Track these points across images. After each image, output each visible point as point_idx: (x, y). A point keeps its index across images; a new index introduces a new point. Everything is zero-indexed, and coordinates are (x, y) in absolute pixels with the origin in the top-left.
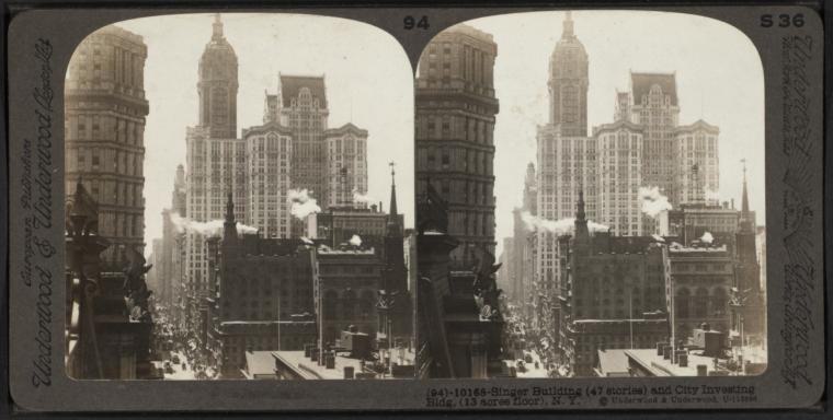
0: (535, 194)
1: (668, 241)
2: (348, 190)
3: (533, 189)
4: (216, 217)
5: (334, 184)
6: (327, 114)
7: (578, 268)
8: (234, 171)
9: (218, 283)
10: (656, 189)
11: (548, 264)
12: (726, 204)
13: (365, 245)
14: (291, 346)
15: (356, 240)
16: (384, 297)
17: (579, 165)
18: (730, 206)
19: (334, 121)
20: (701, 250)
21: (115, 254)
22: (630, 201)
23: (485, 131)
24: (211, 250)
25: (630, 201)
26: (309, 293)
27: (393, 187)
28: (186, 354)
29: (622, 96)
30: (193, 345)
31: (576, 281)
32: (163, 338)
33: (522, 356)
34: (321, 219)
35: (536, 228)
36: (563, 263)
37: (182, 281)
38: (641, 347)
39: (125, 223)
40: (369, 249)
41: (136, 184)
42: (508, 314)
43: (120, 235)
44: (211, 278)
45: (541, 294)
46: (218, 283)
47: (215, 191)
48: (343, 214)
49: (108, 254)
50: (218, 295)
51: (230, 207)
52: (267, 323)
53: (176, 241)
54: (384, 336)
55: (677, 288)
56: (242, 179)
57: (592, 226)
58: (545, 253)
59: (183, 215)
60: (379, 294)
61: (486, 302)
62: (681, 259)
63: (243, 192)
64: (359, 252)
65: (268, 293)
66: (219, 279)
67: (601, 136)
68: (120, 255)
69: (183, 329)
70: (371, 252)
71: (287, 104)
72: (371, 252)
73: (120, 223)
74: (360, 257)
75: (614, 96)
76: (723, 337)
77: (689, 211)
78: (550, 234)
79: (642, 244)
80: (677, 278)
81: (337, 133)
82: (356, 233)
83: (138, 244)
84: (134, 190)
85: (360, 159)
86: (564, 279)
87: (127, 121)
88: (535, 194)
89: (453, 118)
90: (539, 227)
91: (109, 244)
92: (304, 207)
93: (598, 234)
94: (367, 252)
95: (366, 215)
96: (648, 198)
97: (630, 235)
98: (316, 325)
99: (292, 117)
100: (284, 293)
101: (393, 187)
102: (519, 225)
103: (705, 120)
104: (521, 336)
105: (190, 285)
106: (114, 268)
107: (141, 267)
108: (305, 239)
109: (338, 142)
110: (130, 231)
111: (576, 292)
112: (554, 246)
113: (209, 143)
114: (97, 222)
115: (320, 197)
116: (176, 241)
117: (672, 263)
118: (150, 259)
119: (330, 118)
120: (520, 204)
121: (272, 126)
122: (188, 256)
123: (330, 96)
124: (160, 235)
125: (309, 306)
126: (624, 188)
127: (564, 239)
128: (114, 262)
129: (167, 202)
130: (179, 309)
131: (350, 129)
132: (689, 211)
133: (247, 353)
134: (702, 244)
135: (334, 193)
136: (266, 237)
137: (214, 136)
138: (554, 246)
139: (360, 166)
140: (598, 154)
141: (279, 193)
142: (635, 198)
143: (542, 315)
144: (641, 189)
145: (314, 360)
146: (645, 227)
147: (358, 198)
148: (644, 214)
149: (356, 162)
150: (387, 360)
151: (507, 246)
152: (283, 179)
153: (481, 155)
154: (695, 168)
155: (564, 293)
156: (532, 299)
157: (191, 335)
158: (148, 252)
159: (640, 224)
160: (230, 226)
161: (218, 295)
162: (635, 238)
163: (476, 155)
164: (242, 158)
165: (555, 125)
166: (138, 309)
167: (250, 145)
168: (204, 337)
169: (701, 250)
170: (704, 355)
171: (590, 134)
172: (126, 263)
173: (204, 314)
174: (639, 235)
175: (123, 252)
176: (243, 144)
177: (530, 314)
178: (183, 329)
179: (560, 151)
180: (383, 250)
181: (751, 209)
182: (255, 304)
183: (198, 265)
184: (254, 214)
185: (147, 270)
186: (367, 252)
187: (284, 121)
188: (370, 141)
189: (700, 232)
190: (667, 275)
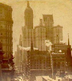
0: (22, 41)
1: (51, 52)
2: (59, 40)
3: (21, 40)
4: (29, 46)
5: (55, 38)
6: (53, 23)
7: (31, 58)
8: (33, 36)
9: (29, 61)
10: (49, 40)
11: (24, 57)
12: (64, 44)
13: (63, 51)
14: (46, 75)
15: (60, 51)
16: (67, 64)
17: (31, 35)
18: (65, 44)
19: (55, 24)
20: (59, 54)
21: (6, 54)
22: (43, 43)
23: (10, 28)
24: (28, 54)
25: (43, 43)
26: (50, 63)
27: (69, 39)
28: (22, 77)
29: (41, 20)
30: (24, 75)
31: (31, 61)
32: (17, 73)
33: (18, 78)
34: (52, 46)
35: (22, 49)
36: (28, 57)
37: (21, 60)
38: (45, 75)
39: (8, 48)
40: (63, 53)
41: (11, 39)
42: (16, 68)
43: (7, 50)
44: (28, 60)
45: (23, 64)
46: (29, 61)
47: (29, 40)
48: (57, 45)
49: (4, 55)
50: (29, 64)
51: (32, 44)
52: (40, 70)
53: (20, 52)
54: (67, 72)
55: (54, 62)
56: (35, 38)
57: (34, 49)
58: (24, 55)
59: (21, 46)
60: (66, 63)
61: (11, 66)
62: (54, 56)
63: (35, 40)
64: (61, 54)
65: (41, 63)
66: (30, 60)
67: (36, 29)
68: (7, 55)
69: (22, 71)
70: (64, 53)
71: (44, 21)
72: (64, 53)
73: (7, 48)
74: (61, 55)
75: (39, 20)
76: (64, 73)
77: (56, 45)
78: (25, 50)
79: (45, 53)
80: (54, 60)
81: (56, 27)
82: (60, 49)
83: (11, 53)
84: (10, 41)
85: (61, 33)
86: (28, 60)
87: (8, 25)
88: (22, 41)
89: (3, 25)
90: (23, 49)
91: (5, 53)
92: (48, 44)
93: (36, 50)
94: (63, 54)
95: (63, 45)
96: (47, 42)
97: (43, 50)
98: (51, 70)
99: (46, 24)
100: (44, 63)
101: (69, 39)
102: (18, 49)
103: (60, 25)
104: (18, 73)
105: (23, 61)
106: (6, 58)
107: (12, 58)
108: (49, 51)
109: (56, 29)
110: (9, 49)
111: (31, 63)
112: (26, 53)
113: (27, 29)
114: (2, 48)
115: (52, 41)
116: (20, 52)
117: (53, 57)
118: (14, 56)
119: (54, 24)
120: (18, 44)
121: (41, 26)
122: (23, 55)
123: (54, 19)
124: (16, 50)
125: (50, 66)
126: (41, 40)
127: (28, 52)
128: (6, 57)
129: (18, 43)
130: (21, 67)
131: (59, 26)
132: (56, 45)
133: (36, 77)
134: (60, 53)
135: (55, 41)
136: (40, 51)
137: (28, 28)
138: (26, 53)
139: (61, 34)
140: (36, 33)
141: (43, 41)
142: (44, 42)
143: (23, 69)
144: (45, 40)
145: (51, 78)
146: (46, 49)
147: (61, 42)
148: (46, 46)
149: (60, 34)
150: (68, 78)
151: (15, 54)
152: (44, 37)
153: (10, 33)
154: (58, 36)
155: (28, 64)
156: (21, 65)
157: (23, 73)
158: (14, 54)
159: (45, 48)
160: (32, 48)
161: (29, 64)
162: (44, 51)
163: (8, 33)
164: (34, 33)
165: (26, 26)
166: (11, 67)
167: (37, 30)
168: (26, 73)
169: (59, 54)
170: (59, 77)
171: (34, 28)
172: (9, 57)
173: (26, 68)
174: (45, 51)
175: (8, 55)
176: (34, 30)
177: (21, 69)
178: (22, 71)
179: (27, 31)
180: (66, 53)
181: (70, 45)
182: (38, 66)
183: (25, 57)
184: (37, 45)
185: (13, 58)
186: (63, 54)
187: (44, 25)
188: (63, 29)
189: (59, 50)
190: (51, 59)
